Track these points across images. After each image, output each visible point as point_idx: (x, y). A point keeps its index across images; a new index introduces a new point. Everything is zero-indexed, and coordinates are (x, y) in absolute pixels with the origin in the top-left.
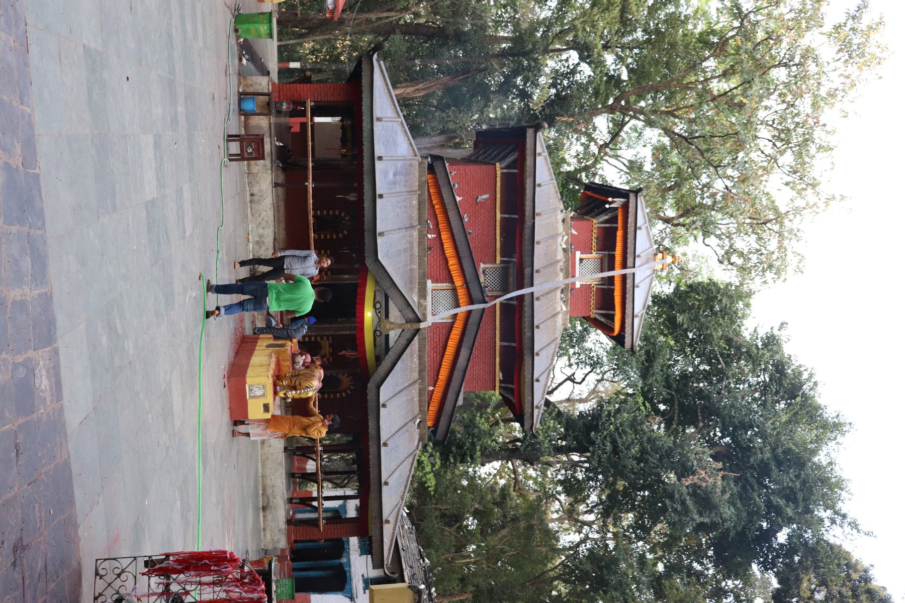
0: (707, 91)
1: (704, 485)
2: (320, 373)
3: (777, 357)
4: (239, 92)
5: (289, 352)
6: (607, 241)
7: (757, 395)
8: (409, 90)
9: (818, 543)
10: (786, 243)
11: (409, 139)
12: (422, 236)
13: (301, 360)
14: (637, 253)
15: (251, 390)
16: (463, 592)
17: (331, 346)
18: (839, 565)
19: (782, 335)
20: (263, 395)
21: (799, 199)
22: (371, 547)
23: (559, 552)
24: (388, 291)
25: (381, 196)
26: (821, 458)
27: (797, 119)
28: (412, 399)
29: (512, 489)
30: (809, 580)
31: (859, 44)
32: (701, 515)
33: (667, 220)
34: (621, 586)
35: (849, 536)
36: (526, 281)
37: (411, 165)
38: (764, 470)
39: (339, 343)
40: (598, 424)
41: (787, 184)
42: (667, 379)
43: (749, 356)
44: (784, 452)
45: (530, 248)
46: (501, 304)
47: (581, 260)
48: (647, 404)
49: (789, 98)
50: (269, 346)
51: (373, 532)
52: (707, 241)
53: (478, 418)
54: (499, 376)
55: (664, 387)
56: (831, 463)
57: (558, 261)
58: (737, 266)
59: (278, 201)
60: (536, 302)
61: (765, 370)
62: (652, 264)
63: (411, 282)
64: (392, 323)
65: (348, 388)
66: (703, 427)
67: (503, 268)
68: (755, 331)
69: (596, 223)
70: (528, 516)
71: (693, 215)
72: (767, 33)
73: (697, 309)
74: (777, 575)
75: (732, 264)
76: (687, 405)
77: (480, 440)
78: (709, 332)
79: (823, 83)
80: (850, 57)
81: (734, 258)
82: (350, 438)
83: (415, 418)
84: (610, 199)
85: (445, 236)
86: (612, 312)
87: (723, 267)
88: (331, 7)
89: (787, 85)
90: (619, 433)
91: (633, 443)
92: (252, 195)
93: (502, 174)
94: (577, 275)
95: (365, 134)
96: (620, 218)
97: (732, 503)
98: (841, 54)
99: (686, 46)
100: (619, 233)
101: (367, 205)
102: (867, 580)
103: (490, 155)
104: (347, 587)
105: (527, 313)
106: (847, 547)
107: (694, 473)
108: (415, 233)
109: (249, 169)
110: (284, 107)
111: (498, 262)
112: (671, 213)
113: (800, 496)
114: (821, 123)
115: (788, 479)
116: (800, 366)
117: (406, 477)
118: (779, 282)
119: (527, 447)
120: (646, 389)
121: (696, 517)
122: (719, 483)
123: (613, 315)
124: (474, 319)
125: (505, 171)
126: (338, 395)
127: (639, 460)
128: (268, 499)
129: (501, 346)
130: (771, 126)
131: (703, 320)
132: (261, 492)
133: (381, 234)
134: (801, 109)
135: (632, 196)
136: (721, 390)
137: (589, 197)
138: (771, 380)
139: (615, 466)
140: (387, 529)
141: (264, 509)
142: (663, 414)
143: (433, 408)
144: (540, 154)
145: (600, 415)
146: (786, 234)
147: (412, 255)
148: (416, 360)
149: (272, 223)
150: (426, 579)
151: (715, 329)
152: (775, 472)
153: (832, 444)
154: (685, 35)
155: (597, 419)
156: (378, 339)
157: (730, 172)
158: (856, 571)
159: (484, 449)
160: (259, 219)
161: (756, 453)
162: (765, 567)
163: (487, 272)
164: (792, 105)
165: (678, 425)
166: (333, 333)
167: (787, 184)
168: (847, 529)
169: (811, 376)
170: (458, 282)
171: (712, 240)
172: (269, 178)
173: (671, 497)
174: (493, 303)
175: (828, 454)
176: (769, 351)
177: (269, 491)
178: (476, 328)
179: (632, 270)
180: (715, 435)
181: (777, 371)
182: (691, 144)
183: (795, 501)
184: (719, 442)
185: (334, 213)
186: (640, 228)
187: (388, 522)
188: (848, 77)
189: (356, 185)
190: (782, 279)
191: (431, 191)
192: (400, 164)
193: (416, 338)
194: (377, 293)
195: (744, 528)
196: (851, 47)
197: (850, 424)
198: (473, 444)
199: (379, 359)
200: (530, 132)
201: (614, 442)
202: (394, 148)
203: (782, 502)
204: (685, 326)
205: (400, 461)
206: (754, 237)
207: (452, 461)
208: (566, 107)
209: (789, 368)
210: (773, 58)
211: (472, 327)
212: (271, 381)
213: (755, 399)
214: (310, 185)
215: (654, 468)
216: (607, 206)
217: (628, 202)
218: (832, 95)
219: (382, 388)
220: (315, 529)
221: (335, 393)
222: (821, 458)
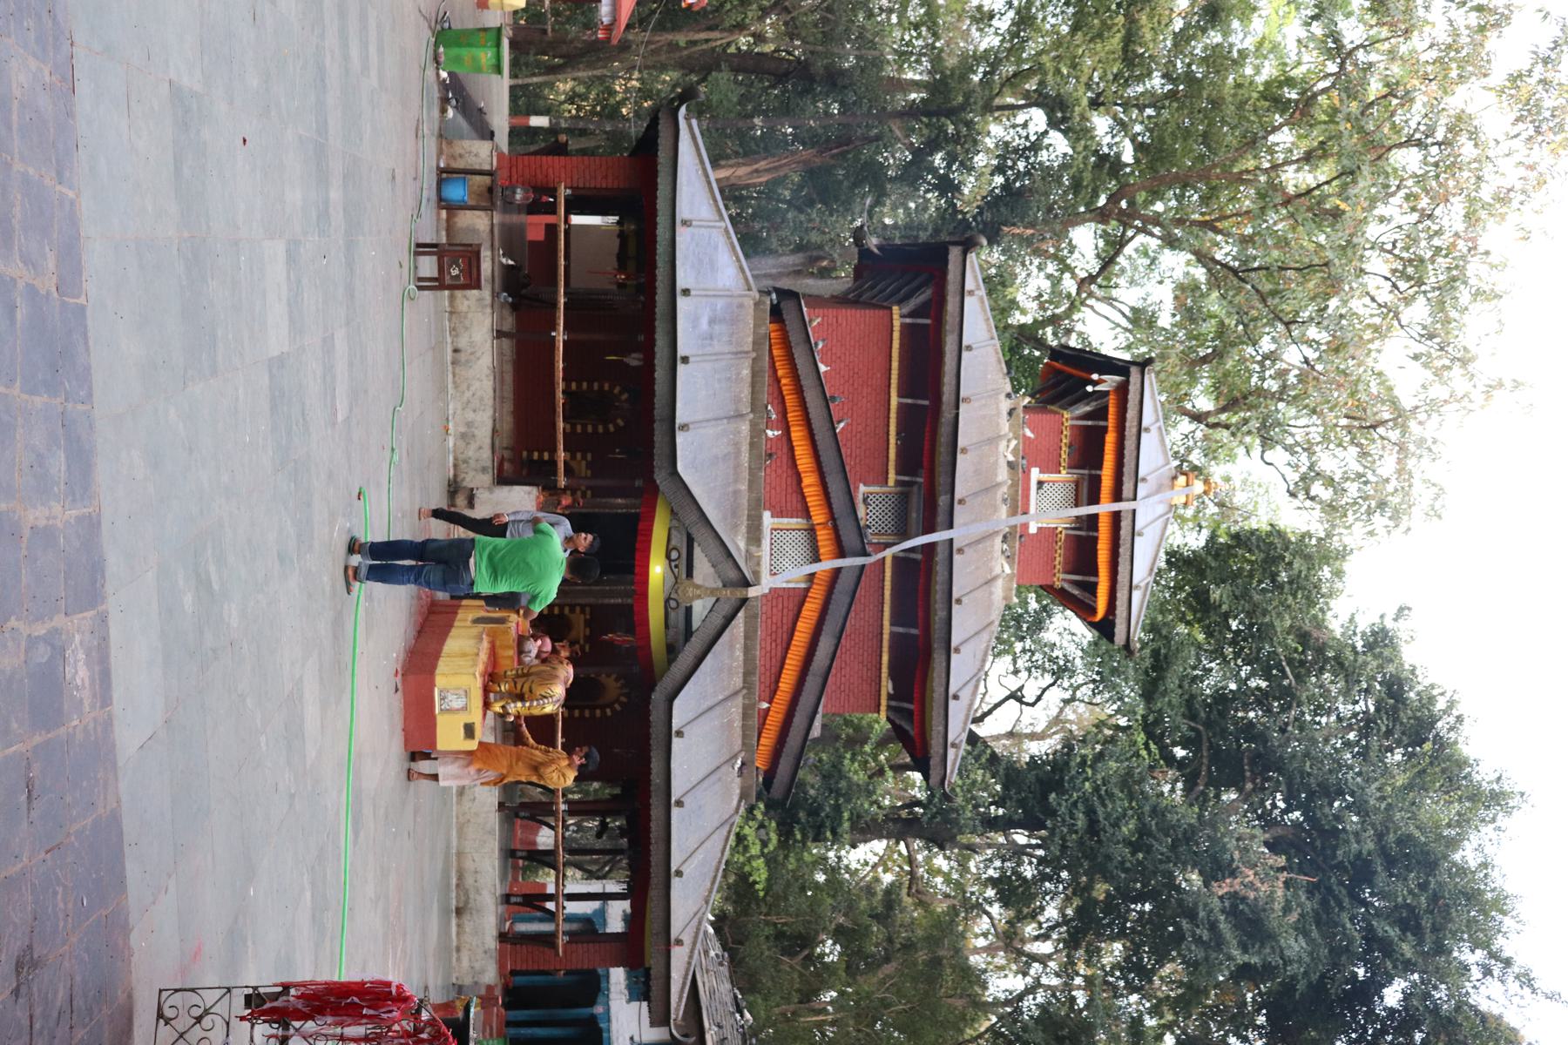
0: (1275, 187)
1: (1252, 895)
2: (567, 672)
3: (1391, 669)
5: (513, 632)
6: (1087, 451)
7: (1352, 736)
8: (742, 171)
9: (1458, 1008)
10: (1411, 463)
11: (738, 260)
12: (756, 432)
13: (533, 647)
14: (1141, 474)
15: (443, 699)
17: (588, 623)
19: (1401, 630)
20: (465, 709)
21: (1437, 385)
23: (986, 1008)
25: (685, 360)
26: (1467, 855)
27: (1436, 242)
28: (731, 722)
29: (905, 891)
33: (1197, 417)
35: (1516, 1000)
36: (941, 518)
37: (741, 306)
38: (1362, 872)
39: (602, 619)
40: (1062, 779)
41: (1416, 357)
43: (1339, 665)
45: (949, 458)
47: (1040, 484)
48: (1153, 747)
49: (1424, 202)
50: (477, 621)
51: (653, 961)
52: (1269, 455)
53: (846, 762)
54: (887, 686)
55: (1184, 716)
56: (1484, 865)
57: (999, 485)
59: (501, 362)
60: (956, 557)
61: (1367, 691)
63: (735, 513)
64: (698, 587)
65: (617, 701)
66: (1254, 790)
67: (902, 493)
68: (1351, 620)
69: (1070, 418)
70: (932, 941)
72: (1387, 85)
73: (1246, 578)
75: (1312, 499)
76: (1227, 749)
77: (848, 801)
78: (1267, 619)
79: (1486, 178)
80: (1538, 131)
81: (1317, 488)
82: (617, 791)
83: (735, 757)
84: (1095, 377)
85: (797, 434)
86: (1093, 579)
87: (1296, 503)
89: (1420, 179)
90: (1100, 797)
91: (1124, 815)
92: (456, 351)
93: (902, 325)
94: (1032, 510)
95: (661, 248)
96: (1112, 410)
97: (1301, 929)
98: (1521, 126)
99: (1241, 106)
100: (1110, 438)
101: (660, 374)
103: (881, 292)
106: (1512, 1019)
107: (1233, 874)
108: (745, 428)
110: (518, 197)
111: (891, 482)
113: (1426, 923)
116: (1432, 686)
117: (714, 863)
118: (1398, 533)
119: (934, 817)
120: (1151, 718)
121: (1236, 953)
122: (1280, 893)
123: (1096, 584)
124: (845, 583)
125: (908, 320)
127: (1135, 847)
129: (892, 634)
130: (1390, 252)
132: (454, 881)
133: (684, 427)
135: (1134, 371)
136: (1287, 724)
137: (1058, 372)
138: (1378, 710)
139: (1090, 855)
140: (679, 956)
143: (768, 740)
144: (971, 293)
145: (1067, 763)
146: (1412, 447)
147: (737, 466)
148: (739, 654)
149: (491, 402)
151: (1279, 615)
152: (1381, 877)
153: (1488, 830)
154: (1238, 86)
155: (1062, 771)
156: (672, 615)
159: (856, 819)
160: (468, 394)
161: (1347, 842)
163: (872, 500)
164: (1430, 216)
165: (1207, 786)
166: (592, 600)
167: (1416, 357)
168: (1513, 986)
169: (1452, 704)
170: (819, 516)
171: (1278, 455)
172: (488, 322)
173: (1192, 915)
174: (880, 556)
175: (1479, 848)
176: (1376, 657)
177: (469, 881)
178: (847, 600)
180: (1274, 806)
181: (1390, 694)
183: (1418, 931)
186: (1147, 430)
187: (679, 942)
188: (1531, 168)
189: (641, 338)
190: (1403, 527)
191: (775, 352)
192: (720, 303)
193: (741, 614)
194: (674, 532)
195: (1323, 976)
196: (1539, 113)
197: (1522, 794)
198: (837, 809)
199: (672, 651)
200: (954, 253)
202: (711, 277)
203: (1393, 932)
204: (1225, 608)
205: (703, 835)
206: (1354, 451)
207: (799, 837)
208: (1022, 209)
209: (1411, 689)
211: (840, 598)
212: (479, 683)
213: (1348, 744)
214: (560, 336)
215: (1161, 861)
216: (1089, 389)
218: (1502, 198)
219: (677, 703)
221: (593, 708)
222: (1467, 855)
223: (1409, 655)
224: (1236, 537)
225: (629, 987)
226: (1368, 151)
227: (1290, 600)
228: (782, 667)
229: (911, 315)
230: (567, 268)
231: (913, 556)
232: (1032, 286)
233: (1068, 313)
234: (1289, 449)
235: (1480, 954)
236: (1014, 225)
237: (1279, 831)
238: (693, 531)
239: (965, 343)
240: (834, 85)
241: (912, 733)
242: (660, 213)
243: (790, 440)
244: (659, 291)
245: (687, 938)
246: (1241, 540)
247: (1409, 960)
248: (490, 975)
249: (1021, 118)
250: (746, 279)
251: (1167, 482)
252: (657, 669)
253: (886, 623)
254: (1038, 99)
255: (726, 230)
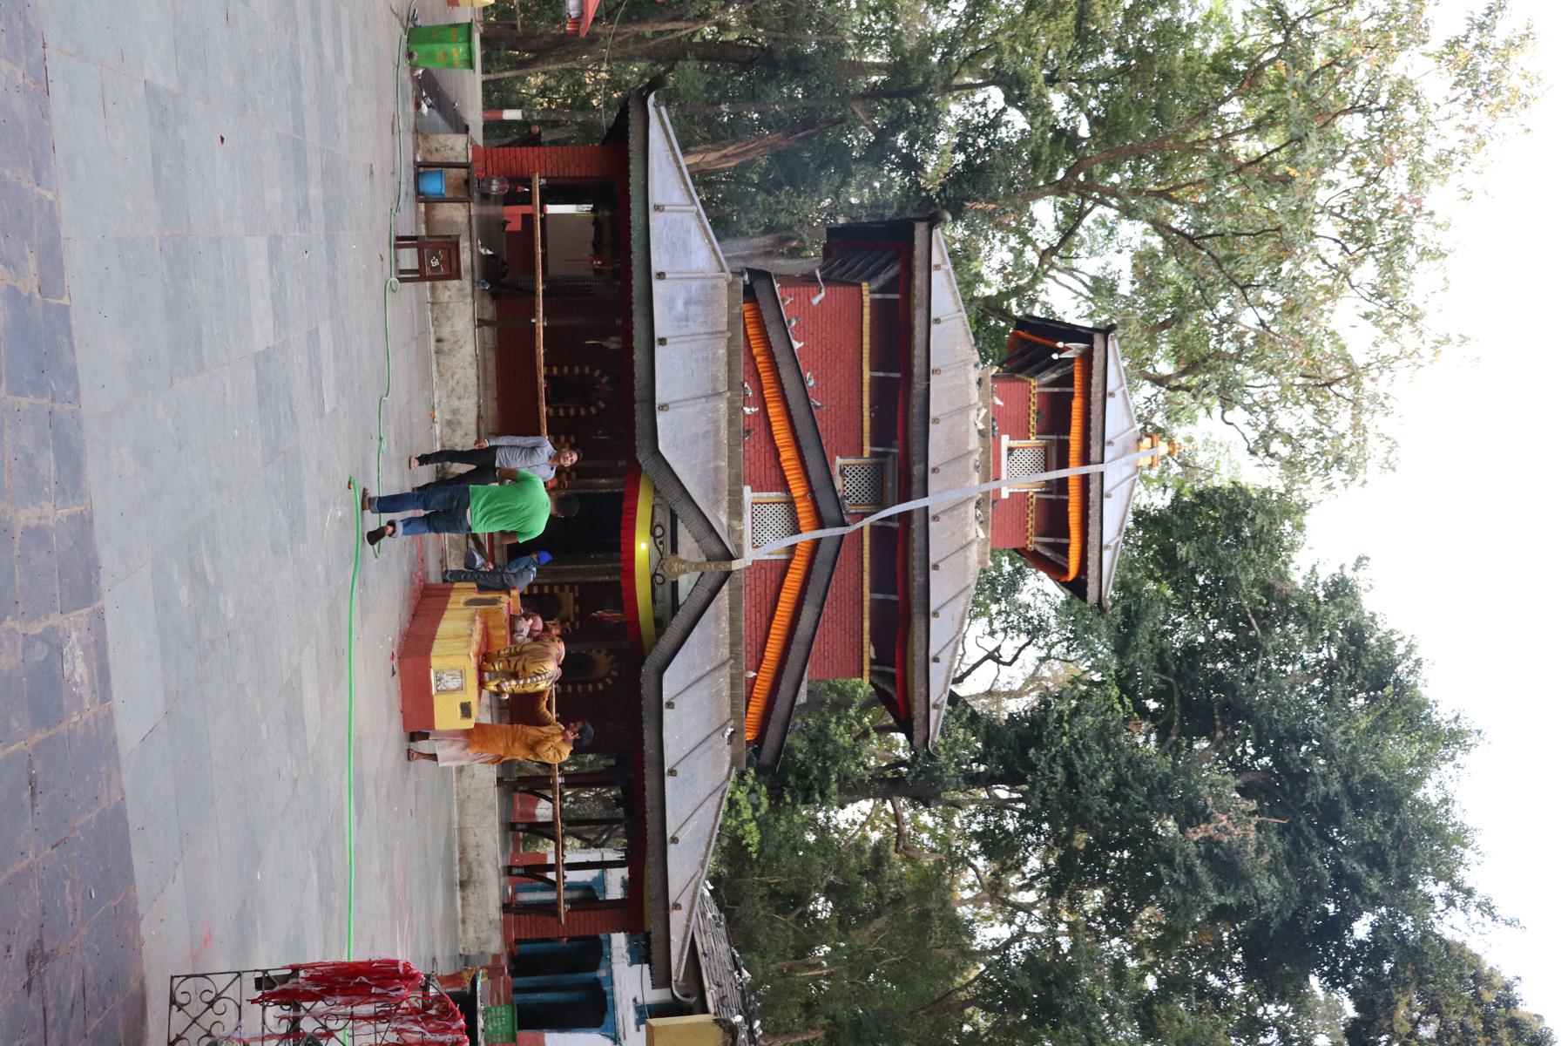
1: (1226, 839)
2: (559, 649)
3: (1352, 617)
4: (415, 162)
5: (505, 611)
6: (1055, 417)
7: (1316, 683)
8: (711, 157)
9: (1424, 938)
10: (1365, 418)
12: (734, 411)
13: (525, 626)
15: (439, 680)
16: (809, 1027)
17: (577, 601)
18: (1460, 978)
19: (1360, 579)
20: (460, 689)
21: (1387, 342)
22: (648, 951)
24: (676, 504)
25: (663, 341)
26: (1429, 792)
27: (1383, 204)
28: (718, 694)
29: (892, 848)
30: (1409, 1004)
31: (1491, 73)
32: (1221, 892)
33: (1159, 381)
34: (1084, 1016)
35: (1478, 928)
36: (916, 487)
37: (715, 287)
38: (1329, 813)
39: (591, 596)
40: (1040, 735)
41: (1367, 316)
42: (1161, 655)
43: (1303, 616)
44: (1365, 782)
46: (872, 527)
47: (1011, 450)
48: (1127, 700)
49: (1370, 167)
50: (470, 603)
51: (653, 926)
52: (1229, 416)
53: (832, 726)
54: (869, 652)
56: (1445, 801)
57: (970, 453)
58: (1280, 459)
59: (483, 350)
60: (932, 524)
61: (1330, 639)
62: (1133, 456)
63: (715, 490)
64: (683, 562)
66: (1224, 738)
68: (1313, 571)
69: (1036, 385)
70: (921, 894)
71: (1204, 371)
72: (1331, 54)
73: (1212, 535)
74: (1353, 995)
75: (1272, 456)
76: (1195, 700)
77: (836, 763)
78: (1232, 574)
82: (612, 762)
83: (723, 726)
84: (1060, 345)
85: (774, 410)
86: (1064, 541)
87: (1257, 460)
88: (574, 14)
89: (1365, 144)
90: (1077, 750)
91: (1101, 767)
92: (439, 340)
93: (873, 301)
95: (635, 234)
96: (1077, 376)
97: (1273, 869)
98: (1459, 90)
100: (1077, 404)
101: (639, 356)
102: (1509, 1003)
104: (608, 1019)
105: (917, 544)
106: (1474, 945)
107: (1207, 819)
108: (723, 406)
109: (433, 296)
110: (494, 188)
111: (866, 454)
112: (1165, 368)
113: (1392, 858)
114: (1426, 210)
115: (1371, 828)
116: (1391, 632)
117: (708, 829)
119: (918, 775)
120: (1124, 673)
121: (1212, 894)
122: (1252, 836)
123: (1067, 545)
124: (825, 553)
125: (878, 296)
126: (590, 687)
127: (1113, 797)
128: (470, 868)
129: (872, 601)
130: (1338, 215)
131: (1221, 553)
132: (457, 856)
133: (664, 407)
134: (1391, 185)
135: (1098, 338)
136: (1254, 674)
137: (1024, 341)
138: (1340, 657)
139: (1070, 807)
140: (677, 920)
141: (463, 885)
142: (1154, 716)
143: (756, 708)
144: (938, 267)
145: (1044, 720)
146: (1365, 403)
147: (717, 444)
148: (725, 625)
150: (744, 1005)
151: (1243, 568)
152: (1348, 815)
153: (1447, 768)
154: (1188, 59)
155: (1040, 727)
156: (659, 590)
157: (1267, 295)
158: (1490, 988)
159: (843, 779)
161: (1315, 784)
162: (1332, 981)
163: (848, 472)
164: (1375, 180)
165: (1179, 736)
166: (581, 579)
167: (1367, 316)
168: (1475, 914)
169: (1410, 649)
170: (798, 490)
171: (1238, 415)
172: (469, 310)
173: (1169, 860)
174: (858, 525)
175: (1440, 786)
176: (1337, 606)
177: (472, 855)
178: (828, 570)
179: (1099, 468)
180: (1244, 752)
181: (1352, 641)
182: (1199, 247)
183: (1384, 867)
184: (1249, 758)
185: (582, 370)
186: (1112, 395)
187: (677, 906)
188: (1471, 130)
189: (619, 322)
190: (1359, 480)
191: (750, 331)
192: (695, 285)
194: (657, 510)
195: (1295, 913)
196: (1476, 77)
198: (825, 771)
199: (660, 625)
200: (920, 229)
201: (1069, 766)
202: (684, 257)
204: (1191, 564)
205: (697, 802)
206: (1310, 408)
207: (788, 800)
208: (982, 185)
210: (1341, 97)
211: (821, 569)
213: (1313, 691)
215: (1138, 810)
216: (1055, 356)
217: (1091, 349)
218: (1444, 161)
219: (666, 675)
220: (551, 920)
222: (1429, 792)
223: (1370, 603)
224: (1200, 495)
225: (630, 951)
226: (1315, 118)
227: (1254, 554)
228: (767, 637)
229: (881, 290)
230: (544, 256)
231: (890, 524)
232: (995, 259)
233: (1032, 284)
234: (1248, 408)
235: (1443, 886)
236: (976, 200)
237: (1249, 777)
238: (677, 508)
239: (933, 316)
240: (797, 70)
241: (895, 696)
242: (633, 199)
243: (767, 417)
244: (635, 275)
245: (684, 902)
246: (1205, 498)
247: (1376, 895)
248: (496, 945)
249: (979, 96)
250: (719, 261)
251: (1133, 445)
252: (646, 643)
253: (866, 590)
254: (997, 78)
255: (698, 214)
